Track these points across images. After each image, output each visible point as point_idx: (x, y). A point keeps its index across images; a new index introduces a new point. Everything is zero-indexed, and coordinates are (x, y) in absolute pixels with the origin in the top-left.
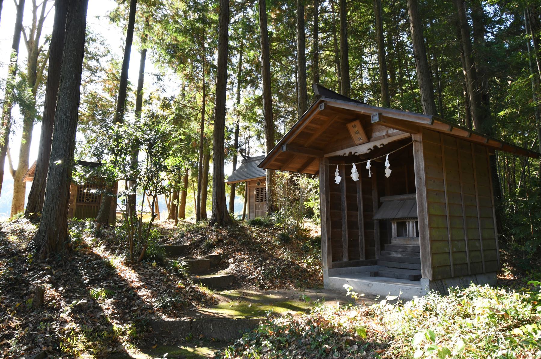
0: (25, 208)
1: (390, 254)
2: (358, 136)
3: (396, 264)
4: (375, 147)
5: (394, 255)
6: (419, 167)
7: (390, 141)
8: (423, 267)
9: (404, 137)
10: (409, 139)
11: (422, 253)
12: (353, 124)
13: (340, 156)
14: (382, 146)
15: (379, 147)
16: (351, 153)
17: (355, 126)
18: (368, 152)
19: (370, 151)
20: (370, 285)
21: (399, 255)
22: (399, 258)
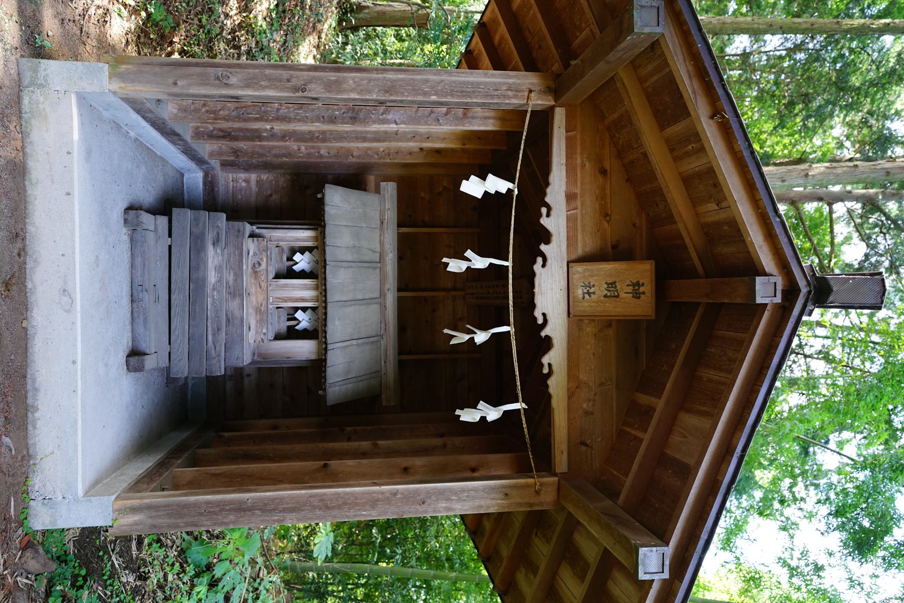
0: (557, 57)
1: (215, 243)
2: (600, 290)
3: (181, 274)
4: (547, 344)
5: (213, 257)
6: (460, 500)
7: (554, 403)
8: (149, 507)
9: (557, 453)
10: (545, 464)
11: (195, 505)
12: (648, 288)
13: (547, 184)
14: (546, 370)
15: (545, 360)
16: (546, 237)
17: (637, 295)
18: (538, 314)
19: (540, 321)
20: (65, 299)
21: (212, 277)
22: (204, 280)
